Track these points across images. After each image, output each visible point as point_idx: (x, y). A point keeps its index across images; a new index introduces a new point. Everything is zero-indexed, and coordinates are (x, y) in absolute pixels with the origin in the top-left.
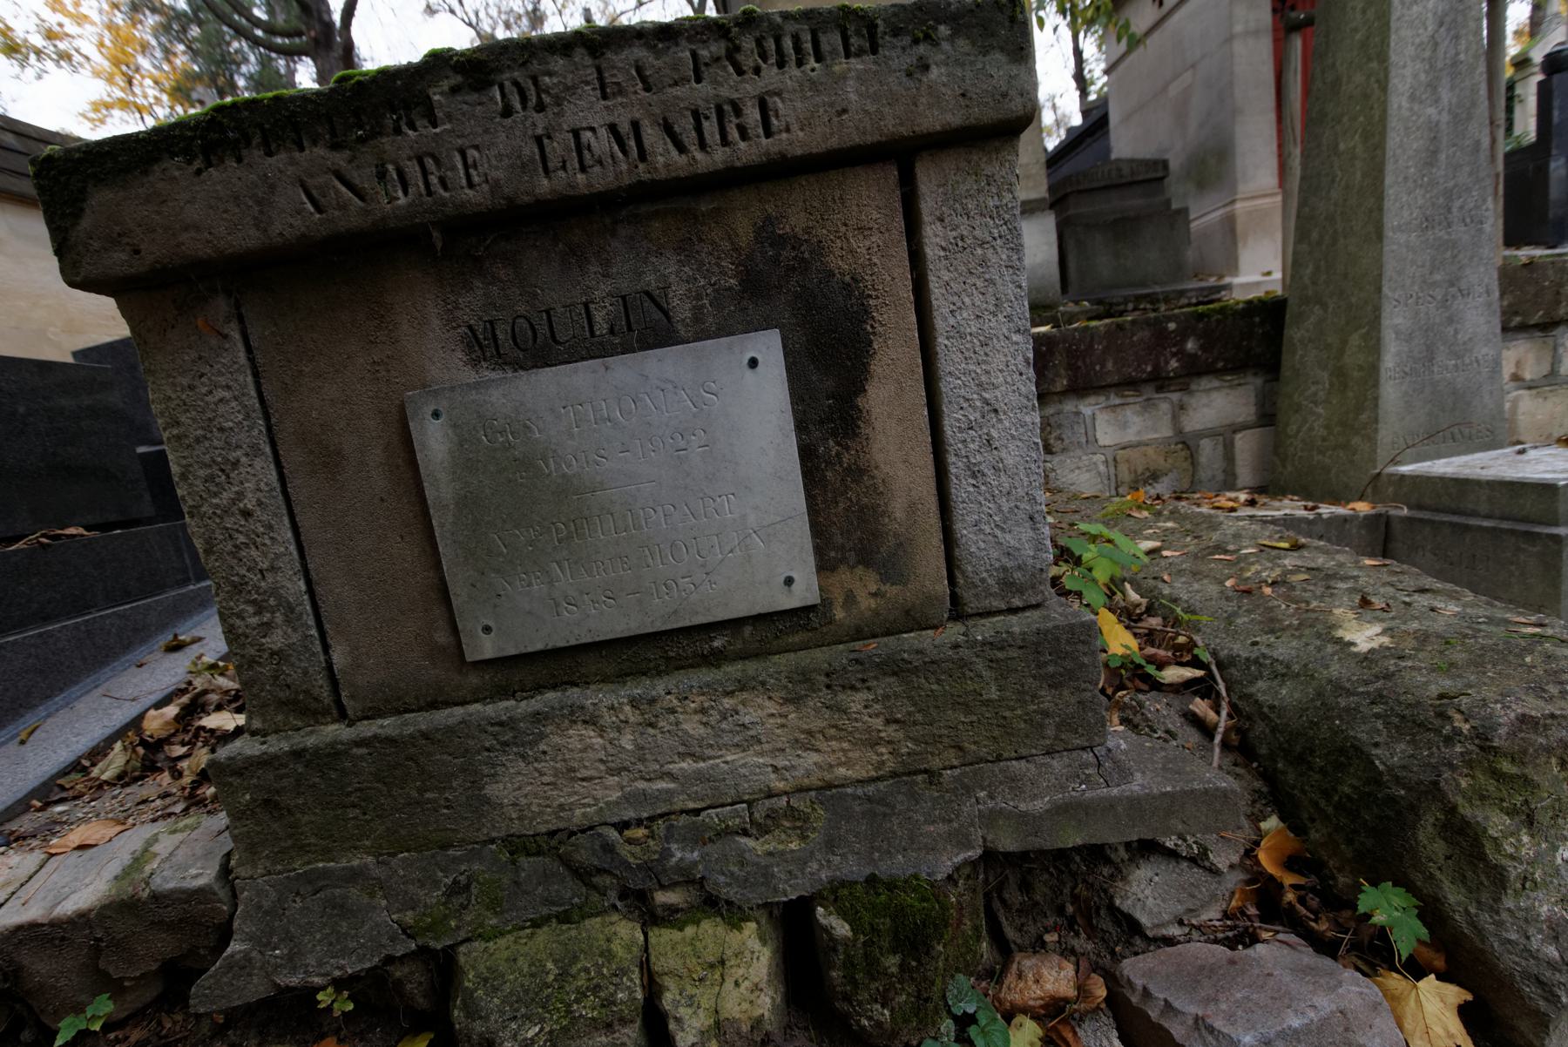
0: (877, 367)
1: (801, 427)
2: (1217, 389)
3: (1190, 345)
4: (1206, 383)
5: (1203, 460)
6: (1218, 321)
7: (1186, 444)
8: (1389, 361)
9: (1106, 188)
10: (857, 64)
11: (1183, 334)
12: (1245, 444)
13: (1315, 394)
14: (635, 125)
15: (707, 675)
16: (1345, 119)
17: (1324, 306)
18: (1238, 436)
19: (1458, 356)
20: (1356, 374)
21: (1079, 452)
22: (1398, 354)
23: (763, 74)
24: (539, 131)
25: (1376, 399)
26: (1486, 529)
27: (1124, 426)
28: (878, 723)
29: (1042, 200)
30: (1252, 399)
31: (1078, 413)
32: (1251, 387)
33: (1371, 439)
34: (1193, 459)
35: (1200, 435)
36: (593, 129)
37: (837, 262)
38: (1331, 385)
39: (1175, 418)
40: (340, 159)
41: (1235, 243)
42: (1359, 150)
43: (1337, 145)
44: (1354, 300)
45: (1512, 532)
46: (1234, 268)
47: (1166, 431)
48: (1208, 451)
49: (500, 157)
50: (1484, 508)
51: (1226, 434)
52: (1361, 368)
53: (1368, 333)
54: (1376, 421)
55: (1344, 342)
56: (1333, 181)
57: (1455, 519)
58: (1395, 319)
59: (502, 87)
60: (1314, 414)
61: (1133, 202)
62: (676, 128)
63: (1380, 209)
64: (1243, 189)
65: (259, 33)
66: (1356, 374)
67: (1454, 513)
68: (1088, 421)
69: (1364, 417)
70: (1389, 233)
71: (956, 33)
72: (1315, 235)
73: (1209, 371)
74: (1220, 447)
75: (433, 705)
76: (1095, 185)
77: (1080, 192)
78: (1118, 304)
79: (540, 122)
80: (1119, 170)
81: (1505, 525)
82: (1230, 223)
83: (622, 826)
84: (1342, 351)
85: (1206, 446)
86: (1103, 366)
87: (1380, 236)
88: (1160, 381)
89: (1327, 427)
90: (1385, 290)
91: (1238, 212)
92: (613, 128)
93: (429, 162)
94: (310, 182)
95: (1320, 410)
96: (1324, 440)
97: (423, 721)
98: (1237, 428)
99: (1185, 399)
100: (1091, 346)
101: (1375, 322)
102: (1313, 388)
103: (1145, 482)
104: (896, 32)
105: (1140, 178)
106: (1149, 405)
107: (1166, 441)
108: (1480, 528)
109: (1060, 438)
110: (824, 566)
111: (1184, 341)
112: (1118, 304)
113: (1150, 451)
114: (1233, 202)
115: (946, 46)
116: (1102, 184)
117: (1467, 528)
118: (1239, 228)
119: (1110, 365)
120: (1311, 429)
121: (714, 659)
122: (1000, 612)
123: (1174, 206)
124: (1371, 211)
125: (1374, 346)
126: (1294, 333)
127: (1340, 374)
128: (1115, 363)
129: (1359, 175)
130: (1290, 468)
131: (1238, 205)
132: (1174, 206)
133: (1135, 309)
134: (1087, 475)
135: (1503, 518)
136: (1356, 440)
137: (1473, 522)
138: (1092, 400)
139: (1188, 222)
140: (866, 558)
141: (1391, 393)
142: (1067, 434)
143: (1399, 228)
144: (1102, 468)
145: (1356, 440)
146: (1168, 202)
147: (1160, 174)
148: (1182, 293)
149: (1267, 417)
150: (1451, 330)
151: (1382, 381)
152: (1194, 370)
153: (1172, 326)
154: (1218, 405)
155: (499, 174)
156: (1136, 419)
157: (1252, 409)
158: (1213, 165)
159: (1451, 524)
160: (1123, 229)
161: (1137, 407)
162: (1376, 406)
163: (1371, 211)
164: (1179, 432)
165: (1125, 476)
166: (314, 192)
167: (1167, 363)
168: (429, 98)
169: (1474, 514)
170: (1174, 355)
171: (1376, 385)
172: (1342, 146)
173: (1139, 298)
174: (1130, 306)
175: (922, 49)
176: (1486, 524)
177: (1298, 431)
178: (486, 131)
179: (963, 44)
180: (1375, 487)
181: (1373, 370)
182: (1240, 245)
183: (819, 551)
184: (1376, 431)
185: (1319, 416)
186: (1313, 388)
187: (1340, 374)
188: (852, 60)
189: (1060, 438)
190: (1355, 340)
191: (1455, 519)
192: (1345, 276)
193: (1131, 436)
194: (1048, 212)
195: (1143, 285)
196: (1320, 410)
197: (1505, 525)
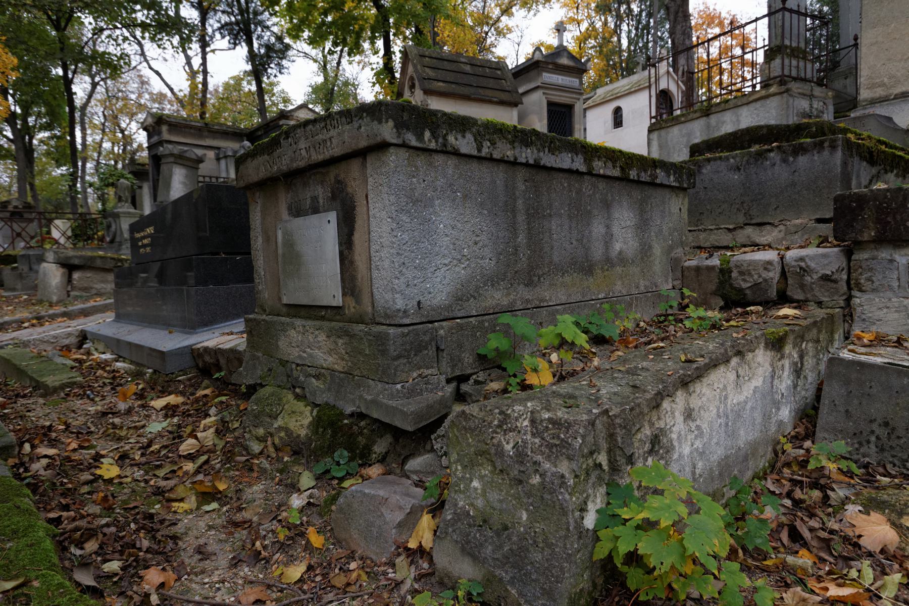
0: (357, 226)
1: (340, 244)
15: (318, 323)
21: (889, 294)
28: (343, 352)
31: (892, 261)
37: (350, 190)
65: (260, 133)
75: (278, 315)
83: (298, 365)
97: (276, 318)
109: (869, 279)
110: (344, 295)
121: (323, 318)
122: (384, 324)
134: (896, 315)
140: (352, 295)
142: (878, 277)
175: (360, 121)
183: (343, 288)
189: (869, 279)
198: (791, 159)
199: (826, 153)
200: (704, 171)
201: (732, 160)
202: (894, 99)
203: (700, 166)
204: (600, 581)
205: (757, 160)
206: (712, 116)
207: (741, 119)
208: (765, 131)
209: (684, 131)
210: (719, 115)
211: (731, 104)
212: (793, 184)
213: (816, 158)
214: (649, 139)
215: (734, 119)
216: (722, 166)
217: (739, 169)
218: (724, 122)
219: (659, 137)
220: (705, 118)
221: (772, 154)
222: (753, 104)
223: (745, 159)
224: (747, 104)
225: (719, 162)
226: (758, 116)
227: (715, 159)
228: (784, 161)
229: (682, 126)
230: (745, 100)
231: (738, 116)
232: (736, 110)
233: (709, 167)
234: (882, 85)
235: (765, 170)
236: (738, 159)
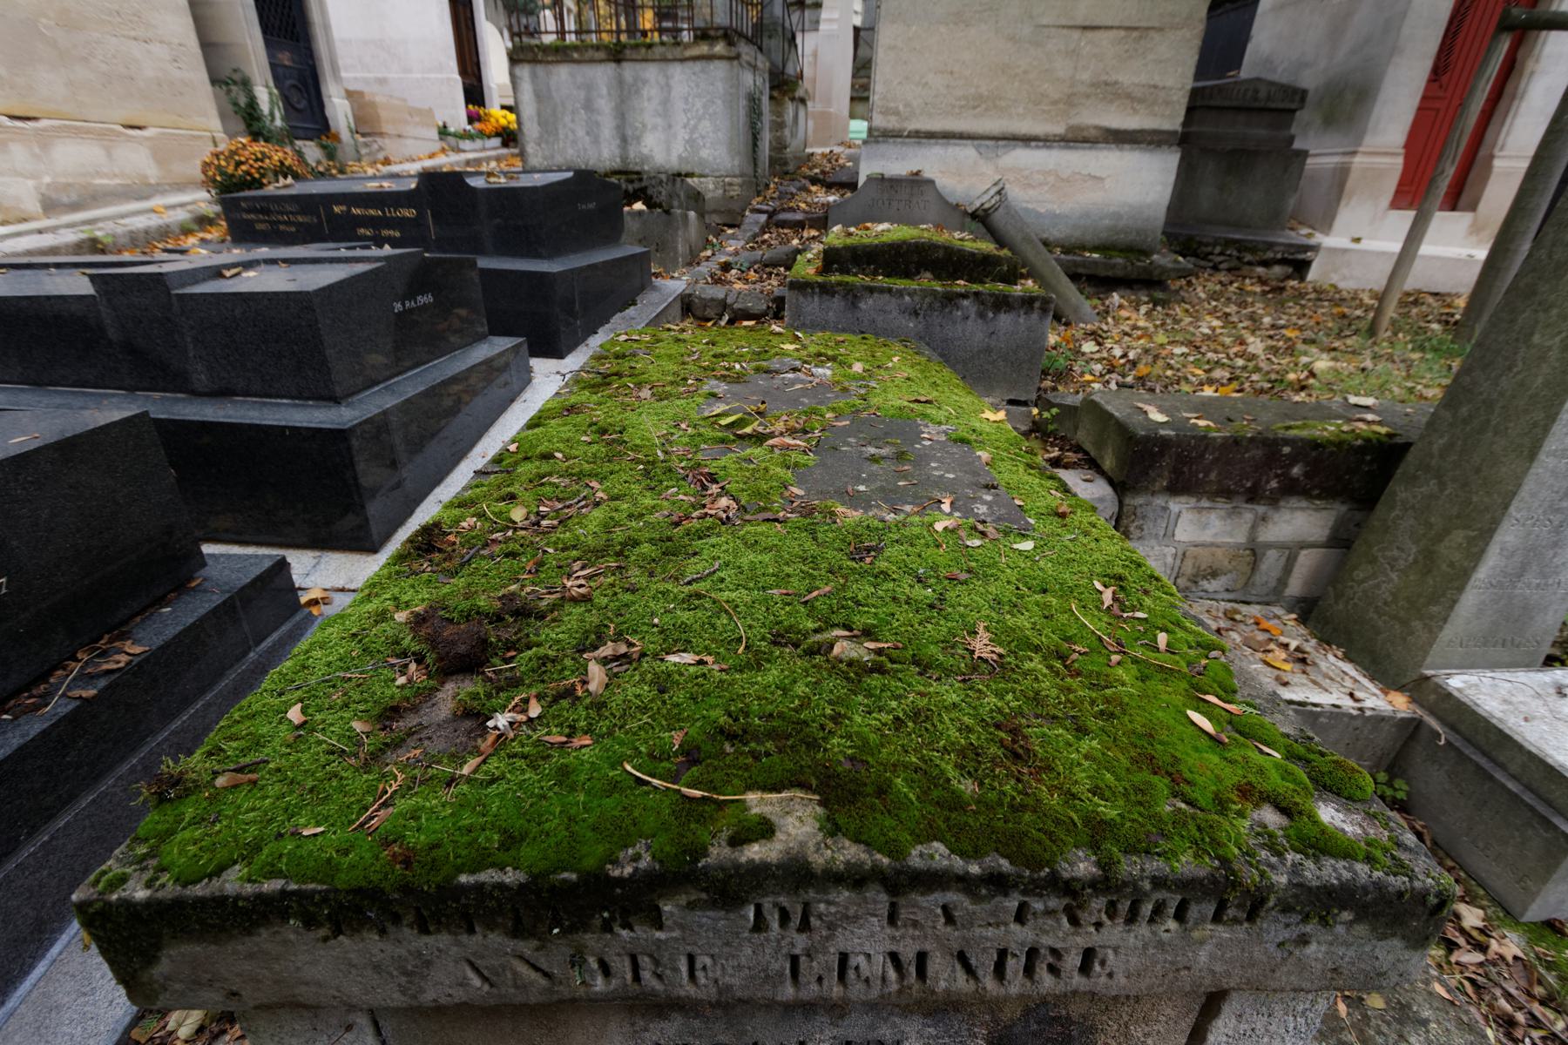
2: (1302, 509)
3: (1296, 471)
4: (1294, 502)
5: (1264, 567)
6: (1332, 453)
7: (1255, 551)
8: (1482, 573)
9: (1238, 109)
10: (1223, 932)
11: (1293, 459)
12: (1306, 561)
13: (1396, 559)
14: (922, 957)
16: (1555, 312)
17: (1442, 486)
18: (1304, 552)
19: (1545, 577)
20: (1444, 567)
21: (1153, 542)
22: (1493, 568)
23: (1102, 930)
24: (797, 951)
25: (1455, 602)
26: (1509, 791)
27: (1205, 526)
29: (1175, 133)
30: (1330, 524)
31: (1165, 509)
32: (1334, 513)
33: (1433, 636)
34: (1254, 566)
35: (1269, 546)
36: (868, 956)
38: (1416, 561)
39: (1254, 527)
40: (527, 947)
41: (1339, 200)
42: (1554, 354)
43: (1532, 334)
44: (1475, 499)
45: (1532, 809)
46: (1326, 224)
47: (1240, 537)
48: (1271, 562)
49: (739, 967)
50: (1514, 768)
51: (1291, 552)
52: (1451, 565)
53: (1474, 538)
54: (1445, 620)
55: (1446, 532)
56: (1510, 369)
57: (1483, 762)
58: (1508, 536)
59: (758, 909)
60: (1385, 577)
61: (1258, 132)
62: (973, 962)
63: (1546, 429)
64: (1370, 141)
66: (1444, 567)
67: (1484, 754)
68: (1173, 517)
69: (1434, 609)
70: (1542, 456)
71: (1358, 919)
72: (1464, 411)
73: (1305, 493)
74: (1283, 559)
76: (1227, 103)
77: (1210, 108)
78: (1207, 245)
79: (801, 942)
80: (1256, 91)
81: (1528, 798)
82: (1342, 174)
84: (1439, 538)
85: (1272, 554)
86: (1206, 475)
87: (1532, 455)
88: (1253, 496)
89: (1393, 595)
90: (1512, 509)
91: (1354, 167)
92: (894, 957)
93: (645, 961)
94: (478, 962)
95: (1394, 576)
96: (1386, 603)
98: (1304, 545)
99: (1270, 513)
100: (1202, 456)
101: (1487, 534)
102: (1396, 553)
103: (1204, 577)
104: (1286, 909)
105: (1273, 105)
106: (1234, 512)
107: (1238, 546)
108: (1503, 787)
111: (1292, 465)
112: (1207, 245)
113: (1219, 552)
114: (1354, 153)
115: (1340, 929)
116: (1235, 103)
117: (1491, 778)
118: (1350, 184)
119: (1213, 476)
120: (1378, 586)
123: (1297, 145)
124: (1535, 425)
125: (1476, 555)
126: (1399, 491)
127: (1428, 559)
128: (1219, 474)
129: (1540, 380)
130: (1341, 607)
131: (1357, 159)
132: (1297, 145)
133: (1221, 254)
135: (1528, 787)
136: (1417, 624)
137: (1499, 776)
138: (1183, 499)
139: (1303, 163)
141: (1470, 600)
142: (1148, 526)
143: (1554, 454)
144: (1170, 560)
145: (1417, 624)
146: (1292, 139)
147: (1293, 106)
148: (1270, 246)
149: (1341, 541)
150: (1551, 553)
151: (1468, 588)
152: (1291, 489)
153: (1286, 450)
154: (1299, 524)
155: (736, 981)
156: (1217, 523)
157: (1327, 532)
158: (1347, 102)
159: (1478, 766)
160: (1239, 160)
161: (1222, 513)
162: (1451, 608)
163: (1535, 425)
164: (1252, 539)
165: (1188, 568)
166: (486, 973)
167: (1268, 482)
168: (658, 909)
169: (1502, 767)
170: (1277, 476)
171: (1461, 589)
172: (1536, 339)
173: (1229, 243)
174: (1218, 250)
176: (1511, 785)
177: (1363, 581)
178: (727, 944)
179: (1361, 929)
180: (1419, 687)
181: (1462, 576)
182: (1343, 203)
184: (1441, 628)
185: (1391, 580)
186: (1396, 553)
187: (1428, 559)
188: (1220, 928)
190: (1459, 536)
191: (1483, 762)
192: (1478, 471)
193: (1207, 536)
194: (1174, 148)
195: (1237, 225)
196: (1394, 576)
197: (1528, 798)
198: (991, 315)
199: (1035, 316)
200: (862, 305)
201: (907, 298)
202: (908, 136)
203: (855, 296)
204: (462, 649)
205: (943, 306)
206: (625, 65)
207: (672, 83)
208: (941, 254)
209: (579, 79)
210: (638, 66)
211: (658, 50)
212: (988, 350)
213: (1021, 320)
214: (512, 75)
215: (662, 80)
216: (892, 304)
217: (916, 314)
218: (645, 82)
219: (534, 76)
220: (613, 65)
221: (966, 303)
222: (690, 64)
223: (927, 300)
224: (683, 60)
225: (887, 296)
226: (697, 86)
227: (882, 290)
228: (982, 315)
229: (575, 67)
230: (677, 52)
231: (667, 77)
232: (663, 65)
233: (870, 302)
234: (897, 113)
235: (954, 323)
236: (917, 298)
